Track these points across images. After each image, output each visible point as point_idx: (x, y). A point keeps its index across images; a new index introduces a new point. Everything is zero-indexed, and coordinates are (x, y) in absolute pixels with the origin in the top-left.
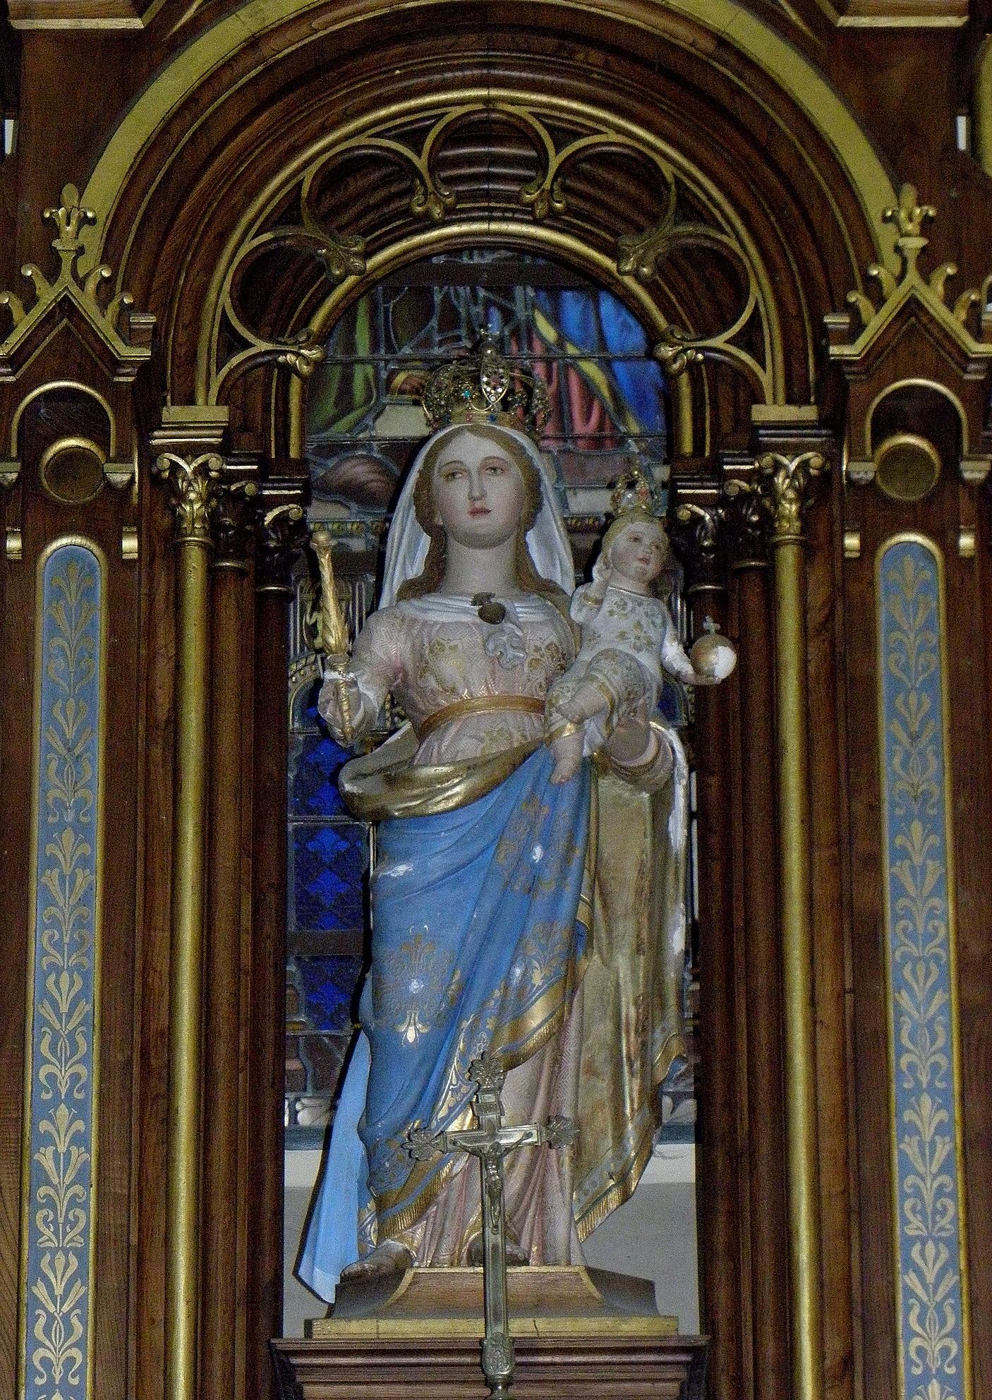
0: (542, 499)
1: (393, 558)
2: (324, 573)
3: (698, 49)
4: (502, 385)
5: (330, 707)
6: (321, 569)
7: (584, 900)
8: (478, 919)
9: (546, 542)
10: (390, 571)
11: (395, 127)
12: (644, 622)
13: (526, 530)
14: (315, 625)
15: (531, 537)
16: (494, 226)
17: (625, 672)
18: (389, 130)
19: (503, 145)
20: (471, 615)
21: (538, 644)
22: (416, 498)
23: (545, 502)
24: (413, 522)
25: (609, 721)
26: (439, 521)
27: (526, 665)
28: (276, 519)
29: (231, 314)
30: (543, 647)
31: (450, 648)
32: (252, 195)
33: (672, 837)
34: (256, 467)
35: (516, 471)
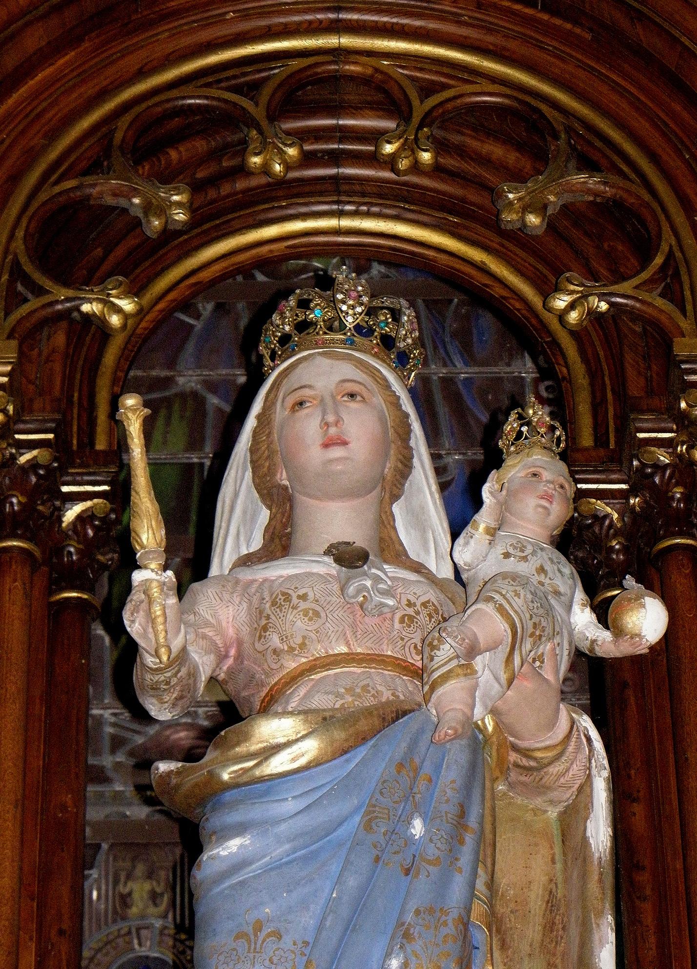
0: (412, 457)
1: (224, 525)
2: (132, 429)
3: (483, 809)
4: (361, 304)
5: (140, 617)
6: (129, 440)
7: (480, 899)
8: (339, 898)
9: (420, 524)
10: (221, 540)
11: (228, 79)
12: (548, 567)
13: (392, 504)
14: (130, 894)
15: (396, 508)
16: (346, 223)
17: (530, 596)
18: (219, 81)
19: (353, 116)
20: (328, 567)
21: (413, 600)
22: (254, 450)
23: (415, 461)
24: (248, 488)
25: (509, 659)
26: (282, 477)
27: (397, 620)
28: (79, 517)
29: (23, 259)
30: (418, 604)
31: (299, 597)
32: (54, 135)
33: (591, 841)
34: (51, 436)
35: (379, 400)
